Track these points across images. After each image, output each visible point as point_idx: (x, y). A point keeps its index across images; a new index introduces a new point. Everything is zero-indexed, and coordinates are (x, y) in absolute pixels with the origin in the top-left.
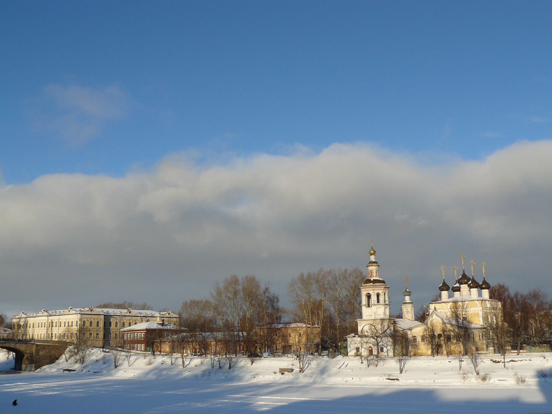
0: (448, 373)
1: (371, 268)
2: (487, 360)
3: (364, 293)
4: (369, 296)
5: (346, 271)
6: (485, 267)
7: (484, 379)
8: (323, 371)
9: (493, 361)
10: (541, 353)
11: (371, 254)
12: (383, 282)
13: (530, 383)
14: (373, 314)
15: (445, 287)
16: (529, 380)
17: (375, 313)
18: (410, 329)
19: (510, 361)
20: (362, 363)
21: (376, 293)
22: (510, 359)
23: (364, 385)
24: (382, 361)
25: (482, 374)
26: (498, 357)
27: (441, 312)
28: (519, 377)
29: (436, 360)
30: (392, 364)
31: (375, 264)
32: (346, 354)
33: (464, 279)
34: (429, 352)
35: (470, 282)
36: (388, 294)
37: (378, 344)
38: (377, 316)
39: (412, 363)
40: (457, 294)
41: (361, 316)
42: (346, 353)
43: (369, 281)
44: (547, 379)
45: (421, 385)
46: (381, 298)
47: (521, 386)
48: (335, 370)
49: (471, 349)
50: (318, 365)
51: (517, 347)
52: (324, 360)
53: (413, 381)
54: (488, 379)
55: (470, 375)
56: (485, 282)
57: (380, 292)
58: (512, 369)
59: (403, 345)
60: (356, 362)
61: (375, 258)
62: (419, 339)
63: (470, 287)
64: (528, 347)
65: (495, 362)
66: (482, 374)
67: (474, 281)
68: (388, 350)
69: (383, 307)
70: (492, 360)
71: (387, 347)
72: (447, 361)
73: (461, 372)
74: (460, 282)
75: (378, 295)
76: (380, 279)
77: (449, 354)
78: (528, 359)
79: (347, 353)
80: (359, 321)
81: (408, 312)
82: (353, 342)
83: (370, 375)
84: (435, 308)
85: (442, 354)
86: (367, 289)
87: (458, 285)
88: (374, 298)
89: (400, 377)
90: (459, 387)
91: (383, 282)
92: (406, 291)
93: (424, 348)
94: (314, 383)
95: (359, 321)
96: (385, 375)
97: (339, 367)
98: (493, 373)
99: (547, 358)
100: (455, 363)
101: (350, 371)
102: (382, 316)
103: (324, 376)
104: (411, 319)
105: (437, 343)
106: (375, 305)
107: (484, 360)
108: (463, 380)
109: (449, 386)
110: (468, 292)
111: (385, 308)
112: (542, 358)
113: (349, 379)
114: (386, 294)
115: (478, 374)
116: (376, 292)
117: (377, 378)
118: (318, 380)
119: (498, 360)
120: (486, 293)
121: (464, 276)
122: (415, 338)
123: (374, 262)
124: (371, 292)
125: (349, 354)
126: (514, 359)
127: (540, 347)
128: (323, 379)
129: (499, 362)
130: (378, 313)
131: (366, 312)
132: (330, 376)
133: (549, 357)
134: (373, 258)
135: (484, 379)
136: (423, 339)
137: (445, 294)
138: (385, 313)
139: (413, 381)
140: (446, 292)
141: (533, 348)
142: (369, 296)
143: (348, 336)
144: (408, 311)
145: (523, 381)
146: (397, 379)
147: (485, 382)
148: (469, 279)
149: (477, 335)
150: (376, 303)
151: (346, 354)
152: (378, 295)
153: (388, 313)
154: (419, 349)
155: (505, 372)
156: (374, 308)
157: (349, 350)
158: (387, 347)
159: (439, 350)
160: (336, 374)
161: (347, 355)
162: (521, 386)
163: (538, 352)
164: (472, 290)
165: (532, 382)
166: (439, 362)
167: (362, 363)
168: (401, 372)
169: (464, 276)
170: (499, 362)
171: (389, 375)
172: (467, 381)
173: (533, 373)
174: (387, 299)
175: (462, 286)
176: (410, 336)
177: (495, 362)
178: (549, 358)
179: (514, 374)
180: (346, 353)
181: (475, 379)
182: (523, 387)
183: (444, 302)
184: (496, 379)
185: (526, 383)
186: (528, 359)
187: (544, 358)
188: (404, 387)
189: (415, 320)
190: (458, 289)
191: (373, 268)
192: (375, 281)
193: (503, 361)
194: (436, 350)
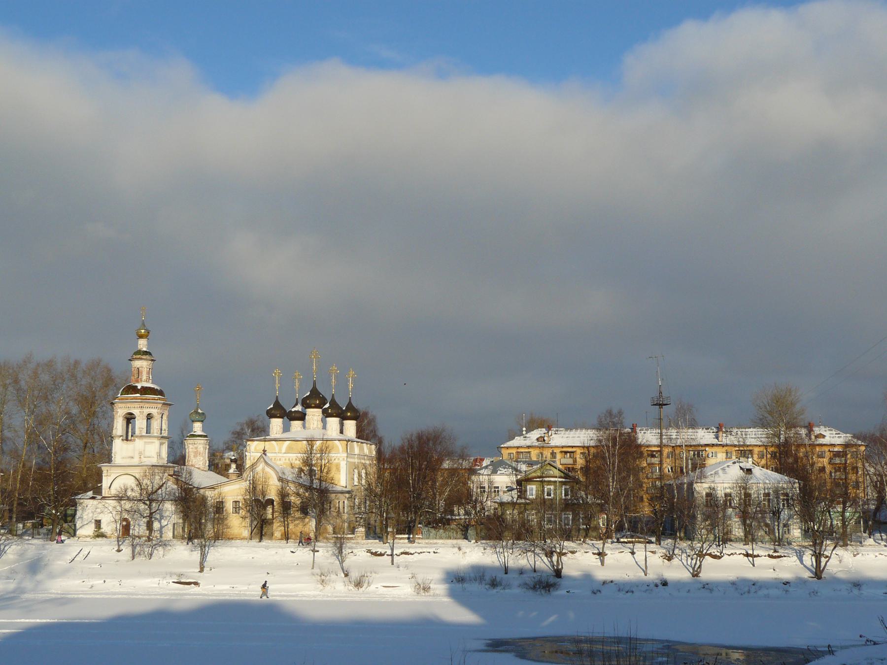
0: (293, 573)
1: (137, 364)
2: (360, 551)
3: (120, 412)
4: (130, 419)
5: (77, 363)
6: (354, 382)
7: (358, 584)
8: (34, 567)
9: (372, 553)
10: (455, 541)
11: (141, 337)
12: (160, 393)
13: (437, 592)
14: (134, 455)
15: (278, 411)
16: (436, 586)
17: (140, 453)
18: (212, 488)
19: (402, 553)
20: (119, 551)
21: (146, 413)
22: (402, 550)
23: (132, 594)
24: (160, 549)
25: (354, 575)
26: (376, 545)
27: (276, 456)
28: (420, 582)
29: (267, 548)
30: (183, 554)
31: (148, 357)
32: (73, 533)
33: (314, 399)
34: (246, 533)
35: (327, 406)
36: (168, 417)
37: (151, 514)
38: (143, 460)
39: (218, 553)
40: (296, 425)
41: (108, 458)
42: (71, 531)
43: (132, 389)
44: (465, 585)
45: (224, 595)
46: (155, 424)
47: (423, 598)
48: (61, 563)
49: (326, 529)
50: (21, 555)
51: (408, 529)
52: (34, 546)
53: (227, 587)
54: (365, 585)
55: (333, 577)
56: (350, 407)
57: (154, 412)
58: (406, 567)
59: (199, 519)
60: (105, 548)
61: (149, 345)
62: (229, 506)
63: (326, 414)
64: (425, 530)
65: (375, 554)
66: (354, 575)
67: (334, 404)
68: (162, 527)
69: (157, 442)
70: (369, 551)
71: (160, 522)
72: (289, 550)
73: (317, 571)
74: (306, 404)
75: (149, 417)
76: (156, 387)
77: (286, 537)
78: (431, 550)
79: (75, 531)
80: (105, 468)
81: (196, 454)
82: (89, 510)
83: (140, 575)
84: (264, 451)
85: (271, 536)
86: (129, 405)
87: (299, 408)
88: (140, 424)
89: (201, 578)
90: (319, 598)
91: (160, 393)
92: (196, 412)
93: (238, 524)
94: (19, 591)
95: (105, 468)
96: (171, 574)
97: (70, 558)
98: (374, 575)
99: (464, 549)
100: (303, 554)
101: (97, 566)
102: (154, 461)
103: (39, 577)
104: (202, 467)
105: (262, 516)
106: (142, 437)
107: (355, 551)
108: (321, 587)
109: (297, 596)
110: (320, 425)
111: (161, 444)
112: (456, 550)
113: (98, 582)
114: (165, 417)
115: (346, 575)
116: (146, 411)
117: (156, 580)
118: (28, 584)
119: (380, 550)
120: (351, 426)
121: (315, 393)
122: (219, 507)
123: (146, 353)
124: (136, 412)
125: (78, 533)
126: (407, 550)
127: (445, 530)
128: (39, 582)
129: (381, 555)
130: (147, 454)
131: (120, 450)
132: (52, 576)
133: (467, 547)
134: (143, 345)
135: (358, 584)
136: (236, 509)
137: (276, 424)
138: (159, 455)
139: (227, 587)
140: (280, 420)
141: (433, 531)
142: (130, 419)
143: (80, 496)
144: (197, 453)
145: (426, 589)
146: (196, 584)
147: (361, 590)
148: (323, 401)
149: (342, 503)
150: (144, 434)
151: (73, 533)
152: (149, 417)
153: (164, 454)
154: (228, 527)
155: (394, 572)
156: (139, 444)
157: (78, 526)
158: (160, 522)
159: (265, 530)
160: (65, 573)
161: (75, 535)
162: (423, 598)
163: (441, 538)
164: (329, 419)
165: (440, 589)
166: (273, 551)
167: (119, 551)
168: (202, 570)
169: (315, 393)
170: (381, 555)
171: (180, 575)
172: (328, 588)
173: (437, 575)
174: (164, 427)
175: (309, 411)
176: (210, 502)
177: (375, 554)
178: (467, 550)
179: (410, 576)
180: (71, 531)
181: (342, 584)
182: (430, 599)
183: (275, 440)
184: (379, 585)
185: (431, 592)
186: (431, 550)
187: (460, 549)
188: (215, 598)
189: (210, 469)
190: (302, 417)
191: (142, 364)
192: (145, 391)
193: (389, 552)
194: (261, 529)
